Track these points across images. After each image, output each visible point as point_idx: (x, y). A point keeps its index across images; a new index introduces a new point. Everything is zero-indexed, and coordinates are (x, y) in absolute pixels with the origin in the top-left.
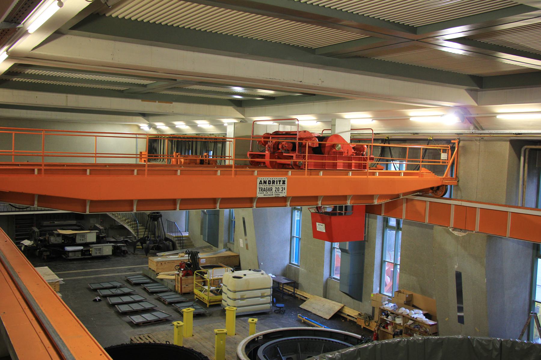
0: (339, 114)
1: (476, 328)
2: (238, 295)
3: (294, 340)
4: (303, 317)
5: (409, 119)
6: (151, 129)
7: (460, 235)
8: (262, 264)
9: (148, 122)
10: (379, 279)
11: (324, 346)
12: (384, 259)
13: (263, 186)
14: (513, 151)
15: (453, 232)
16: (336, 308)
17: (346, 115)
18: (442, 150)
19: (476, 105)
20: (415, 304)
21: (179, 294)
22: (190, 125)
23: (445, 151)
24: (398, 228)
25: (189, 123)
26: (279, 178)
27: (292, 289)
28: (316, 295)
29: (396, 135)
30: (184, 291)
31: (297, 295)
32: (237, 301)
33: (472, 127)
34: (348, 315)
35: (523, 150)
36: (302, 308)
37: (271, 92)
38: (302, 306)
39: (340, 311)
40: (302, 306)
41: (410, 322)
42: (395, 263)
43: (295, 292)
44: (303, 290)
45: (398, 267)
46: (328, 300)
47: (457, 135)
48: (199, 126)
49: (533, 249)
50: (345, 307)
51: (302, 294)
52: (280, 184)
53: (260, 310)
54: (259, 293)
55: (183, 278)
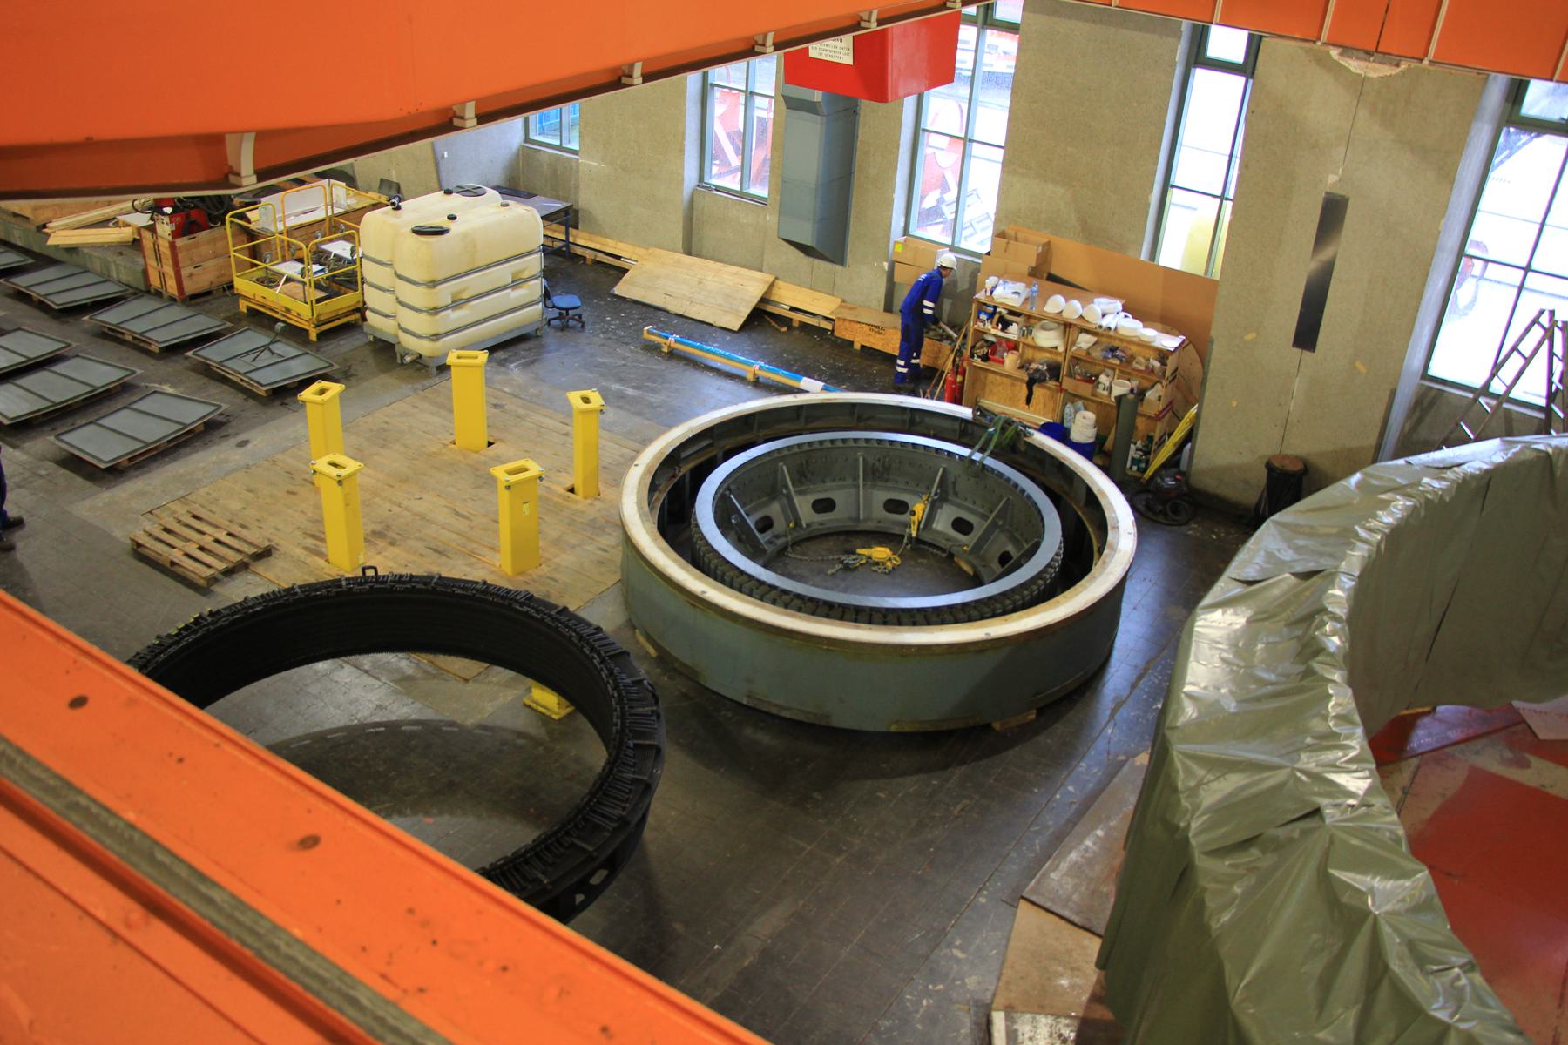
1: (1358, 364)
2: (444, 294)
3: (768, 458)
4: (667, 338)
7: (1375, 75)
11: (864, 459)
15: (1345, 62)
16: (751, 289)
20: (1055, 271)
21: (173, 300)
24: (1247, 68)
27: (559, 232)
28: (656, 247)
30: (190, 287)
31: (579, 251)
32: (442, 314)
34: (793, 309)
36: (624, 299)
38: (619, 290)
39: (767, 297)
40: (619, 290)
41: (1085, 341)
43: (571, 240)
44: (596, 230)
46: (711, 264)
50: (779, 283)
51: (598, 247)
53: (511, 331)
54: (504, 274)
55: (180, 242)
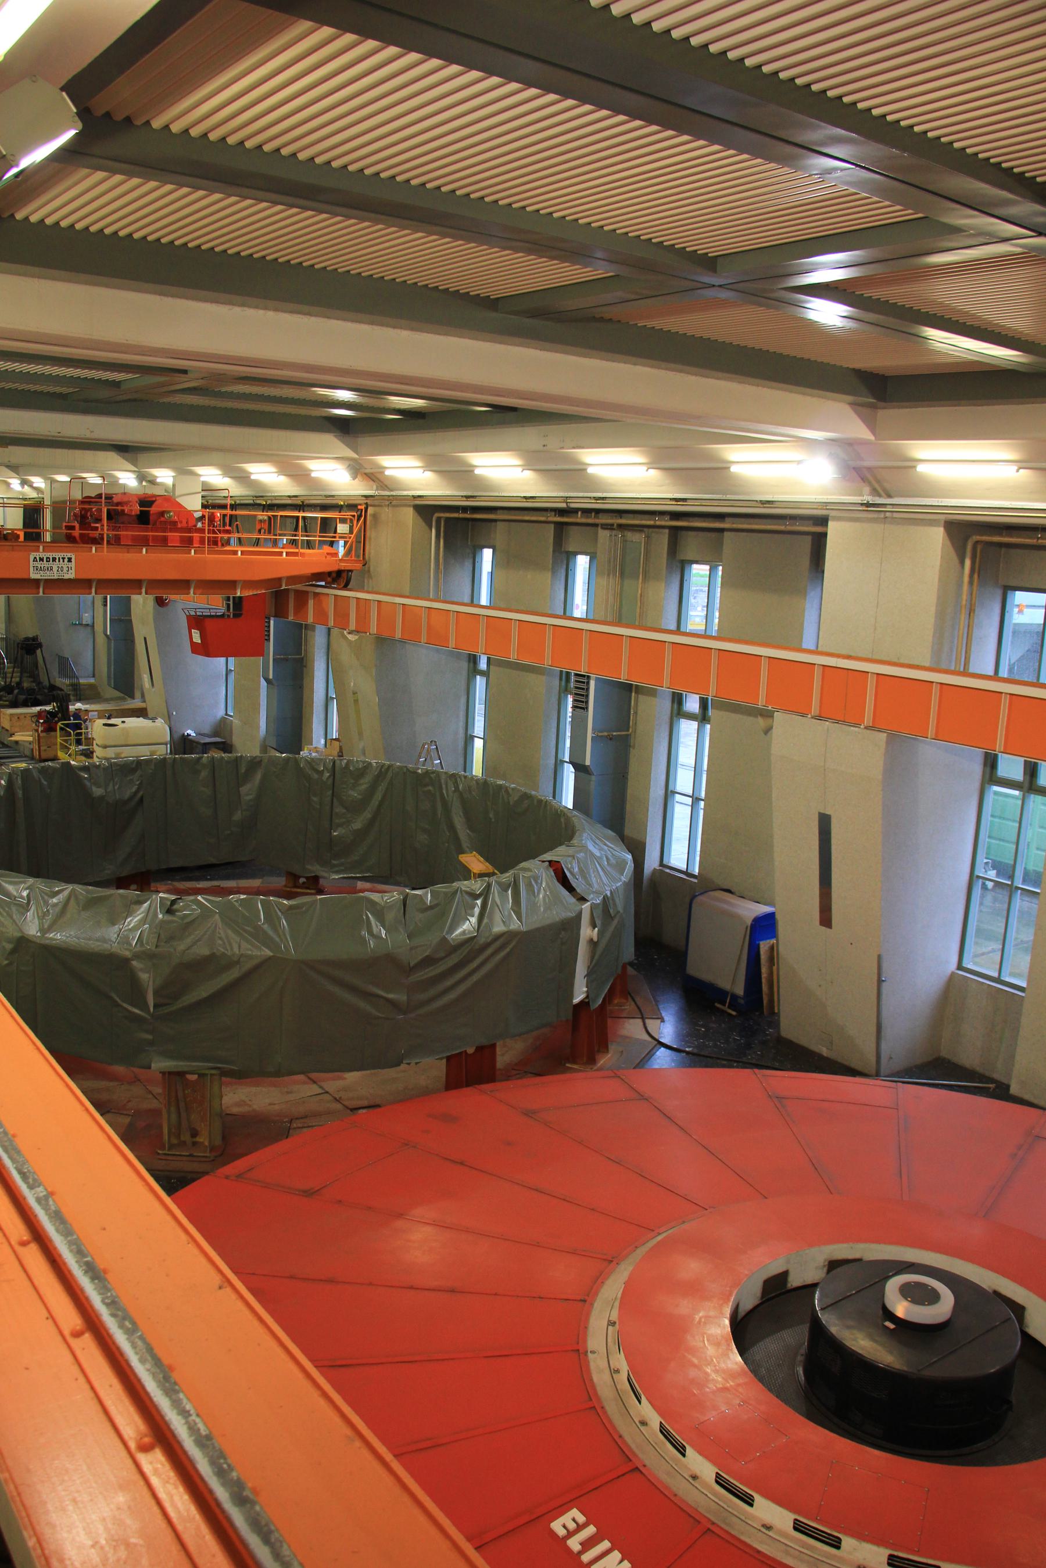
0: (712, 448)
5: (729, 468)
6: (26, 486)
8: (174, 713)
9: (136, 469)
10: (324, 726)
12: (671, 788)
13: (39, 564)
14: (948, 543)
17: (199, 470)
18: (338, 520)
19: (870, 437)
22: (233, 475)
23: (343, 521)
25: (229, 471)
26: (62, 554)
29: (312, 498)
33: (867, 489)
35: (434, 519)
37: (418, 403)
42: (695, 796)
45: (702, 804)
47: (762, 506)
48: (253, 477)
49: (469, 661)
52: (63, 561)
